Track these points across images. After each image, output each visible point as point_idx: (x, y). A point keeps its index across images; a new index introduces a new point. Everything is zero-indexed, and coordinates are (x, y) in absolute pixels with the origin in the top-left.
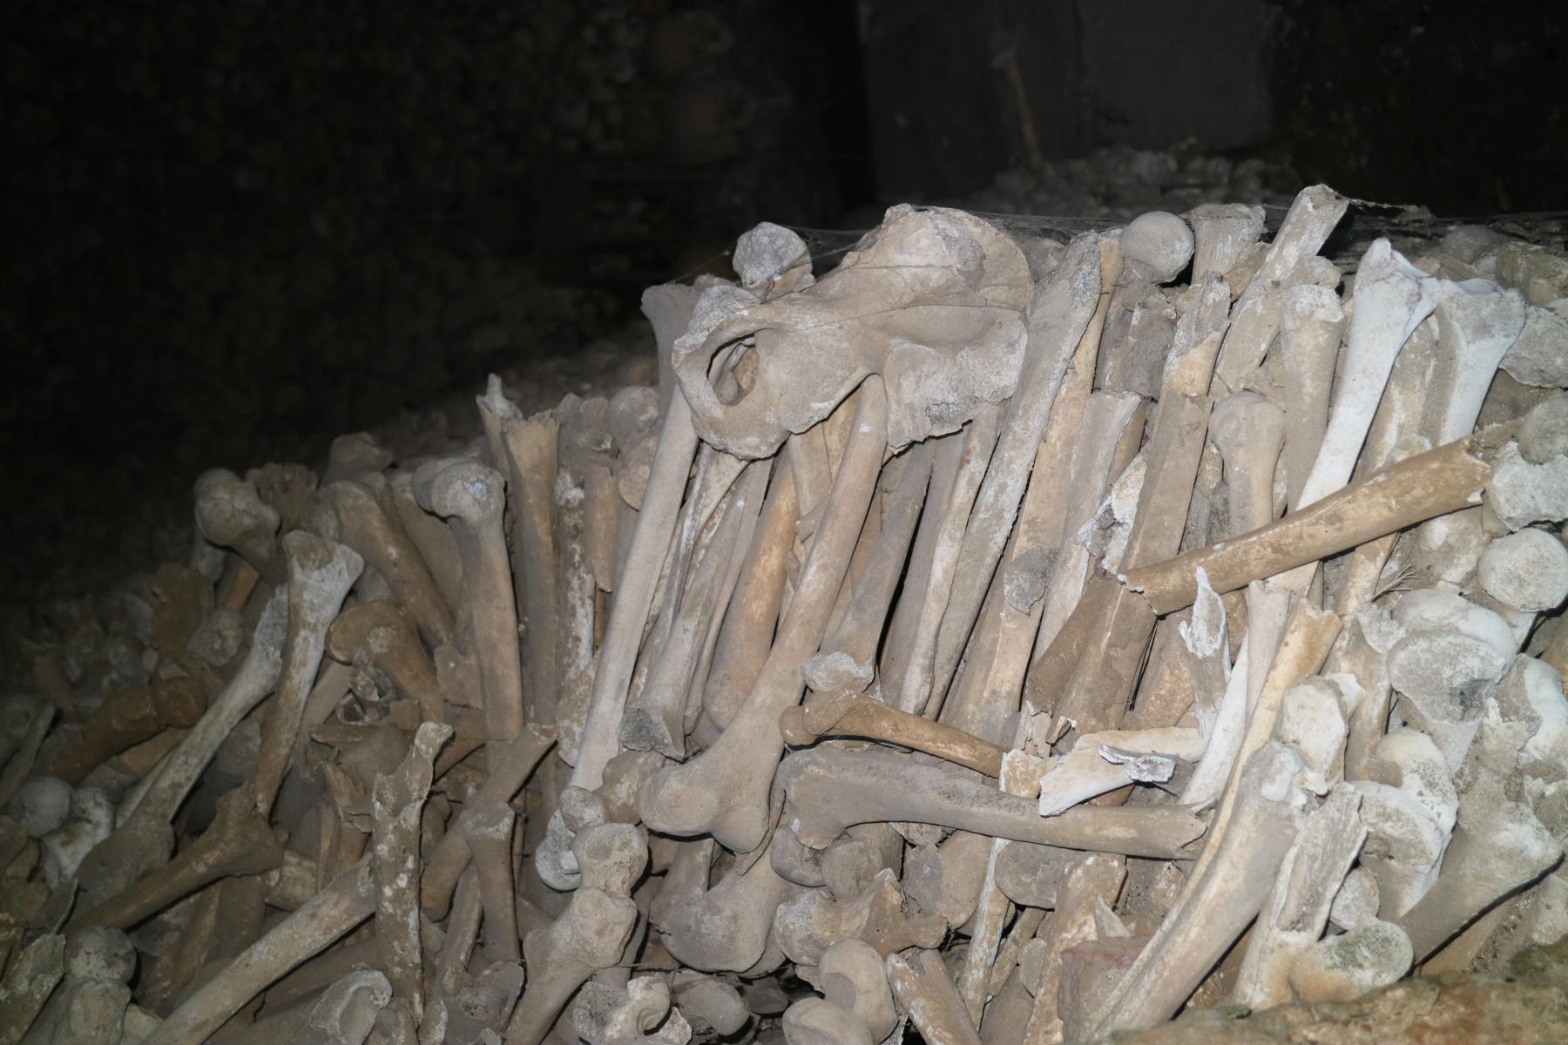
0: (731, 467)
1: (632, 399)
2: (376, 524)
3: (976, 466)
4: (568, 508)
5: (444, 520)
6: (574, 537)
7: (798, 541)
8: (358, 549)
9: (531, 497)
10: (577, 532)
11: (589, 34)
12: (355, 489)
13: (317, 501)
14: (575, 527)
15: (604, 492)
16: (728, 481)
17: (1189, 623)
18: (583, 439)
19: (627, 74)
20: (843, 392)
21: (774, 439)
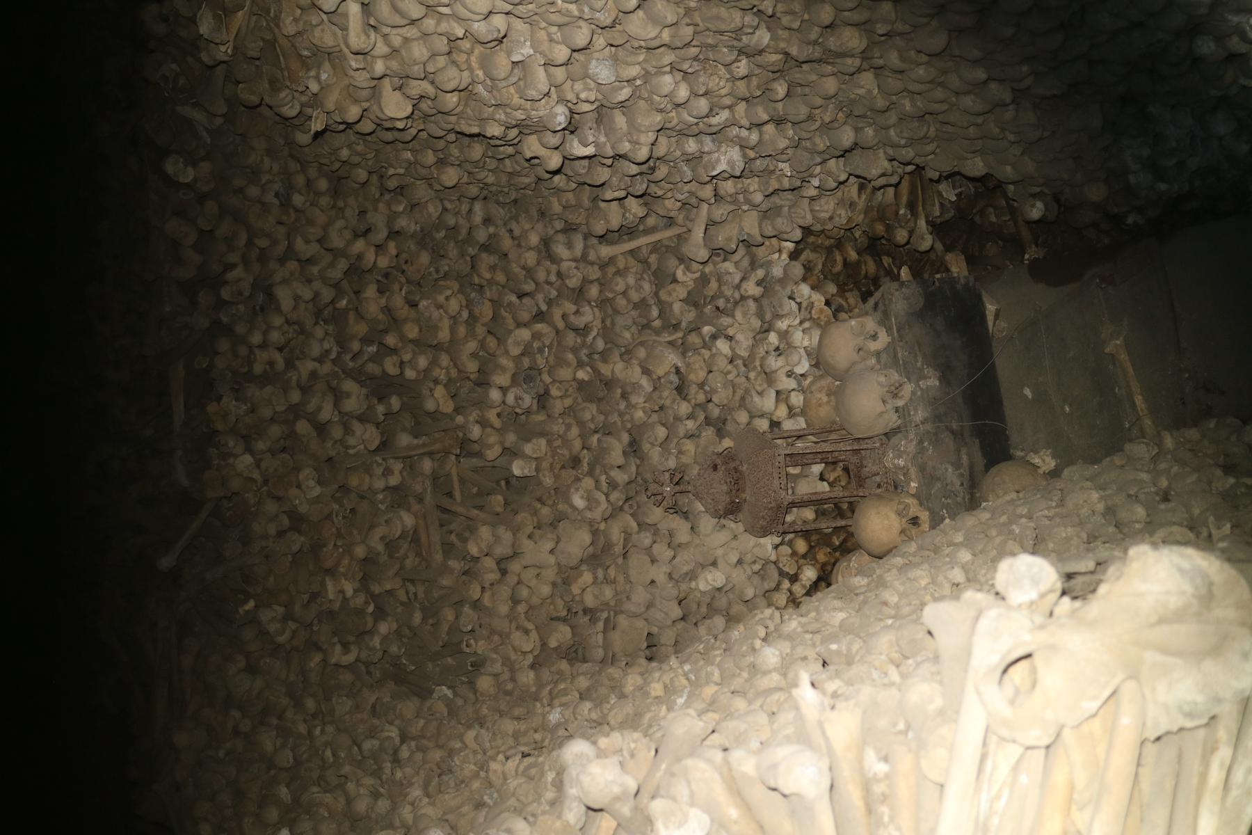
0: (1015, 751)
1: (923, 693)
2: (719, 792)
3: (1224, 753)
4: (876, 779)
5: (785, 796)
6: (883, 802)
7: (1074, 807)
8: (707, 810)
9: (847, 772)
10: (884, 798)
11: (773, 338)
12: (702, 765)
13: (673, 775)
14: (883, 794)
15: (905, 762)
16: (1013, 761)
17: (1076, 586)
18: (883, 723)
19: (803, 367)
20: (1106, 693)
21: (1052, 731)
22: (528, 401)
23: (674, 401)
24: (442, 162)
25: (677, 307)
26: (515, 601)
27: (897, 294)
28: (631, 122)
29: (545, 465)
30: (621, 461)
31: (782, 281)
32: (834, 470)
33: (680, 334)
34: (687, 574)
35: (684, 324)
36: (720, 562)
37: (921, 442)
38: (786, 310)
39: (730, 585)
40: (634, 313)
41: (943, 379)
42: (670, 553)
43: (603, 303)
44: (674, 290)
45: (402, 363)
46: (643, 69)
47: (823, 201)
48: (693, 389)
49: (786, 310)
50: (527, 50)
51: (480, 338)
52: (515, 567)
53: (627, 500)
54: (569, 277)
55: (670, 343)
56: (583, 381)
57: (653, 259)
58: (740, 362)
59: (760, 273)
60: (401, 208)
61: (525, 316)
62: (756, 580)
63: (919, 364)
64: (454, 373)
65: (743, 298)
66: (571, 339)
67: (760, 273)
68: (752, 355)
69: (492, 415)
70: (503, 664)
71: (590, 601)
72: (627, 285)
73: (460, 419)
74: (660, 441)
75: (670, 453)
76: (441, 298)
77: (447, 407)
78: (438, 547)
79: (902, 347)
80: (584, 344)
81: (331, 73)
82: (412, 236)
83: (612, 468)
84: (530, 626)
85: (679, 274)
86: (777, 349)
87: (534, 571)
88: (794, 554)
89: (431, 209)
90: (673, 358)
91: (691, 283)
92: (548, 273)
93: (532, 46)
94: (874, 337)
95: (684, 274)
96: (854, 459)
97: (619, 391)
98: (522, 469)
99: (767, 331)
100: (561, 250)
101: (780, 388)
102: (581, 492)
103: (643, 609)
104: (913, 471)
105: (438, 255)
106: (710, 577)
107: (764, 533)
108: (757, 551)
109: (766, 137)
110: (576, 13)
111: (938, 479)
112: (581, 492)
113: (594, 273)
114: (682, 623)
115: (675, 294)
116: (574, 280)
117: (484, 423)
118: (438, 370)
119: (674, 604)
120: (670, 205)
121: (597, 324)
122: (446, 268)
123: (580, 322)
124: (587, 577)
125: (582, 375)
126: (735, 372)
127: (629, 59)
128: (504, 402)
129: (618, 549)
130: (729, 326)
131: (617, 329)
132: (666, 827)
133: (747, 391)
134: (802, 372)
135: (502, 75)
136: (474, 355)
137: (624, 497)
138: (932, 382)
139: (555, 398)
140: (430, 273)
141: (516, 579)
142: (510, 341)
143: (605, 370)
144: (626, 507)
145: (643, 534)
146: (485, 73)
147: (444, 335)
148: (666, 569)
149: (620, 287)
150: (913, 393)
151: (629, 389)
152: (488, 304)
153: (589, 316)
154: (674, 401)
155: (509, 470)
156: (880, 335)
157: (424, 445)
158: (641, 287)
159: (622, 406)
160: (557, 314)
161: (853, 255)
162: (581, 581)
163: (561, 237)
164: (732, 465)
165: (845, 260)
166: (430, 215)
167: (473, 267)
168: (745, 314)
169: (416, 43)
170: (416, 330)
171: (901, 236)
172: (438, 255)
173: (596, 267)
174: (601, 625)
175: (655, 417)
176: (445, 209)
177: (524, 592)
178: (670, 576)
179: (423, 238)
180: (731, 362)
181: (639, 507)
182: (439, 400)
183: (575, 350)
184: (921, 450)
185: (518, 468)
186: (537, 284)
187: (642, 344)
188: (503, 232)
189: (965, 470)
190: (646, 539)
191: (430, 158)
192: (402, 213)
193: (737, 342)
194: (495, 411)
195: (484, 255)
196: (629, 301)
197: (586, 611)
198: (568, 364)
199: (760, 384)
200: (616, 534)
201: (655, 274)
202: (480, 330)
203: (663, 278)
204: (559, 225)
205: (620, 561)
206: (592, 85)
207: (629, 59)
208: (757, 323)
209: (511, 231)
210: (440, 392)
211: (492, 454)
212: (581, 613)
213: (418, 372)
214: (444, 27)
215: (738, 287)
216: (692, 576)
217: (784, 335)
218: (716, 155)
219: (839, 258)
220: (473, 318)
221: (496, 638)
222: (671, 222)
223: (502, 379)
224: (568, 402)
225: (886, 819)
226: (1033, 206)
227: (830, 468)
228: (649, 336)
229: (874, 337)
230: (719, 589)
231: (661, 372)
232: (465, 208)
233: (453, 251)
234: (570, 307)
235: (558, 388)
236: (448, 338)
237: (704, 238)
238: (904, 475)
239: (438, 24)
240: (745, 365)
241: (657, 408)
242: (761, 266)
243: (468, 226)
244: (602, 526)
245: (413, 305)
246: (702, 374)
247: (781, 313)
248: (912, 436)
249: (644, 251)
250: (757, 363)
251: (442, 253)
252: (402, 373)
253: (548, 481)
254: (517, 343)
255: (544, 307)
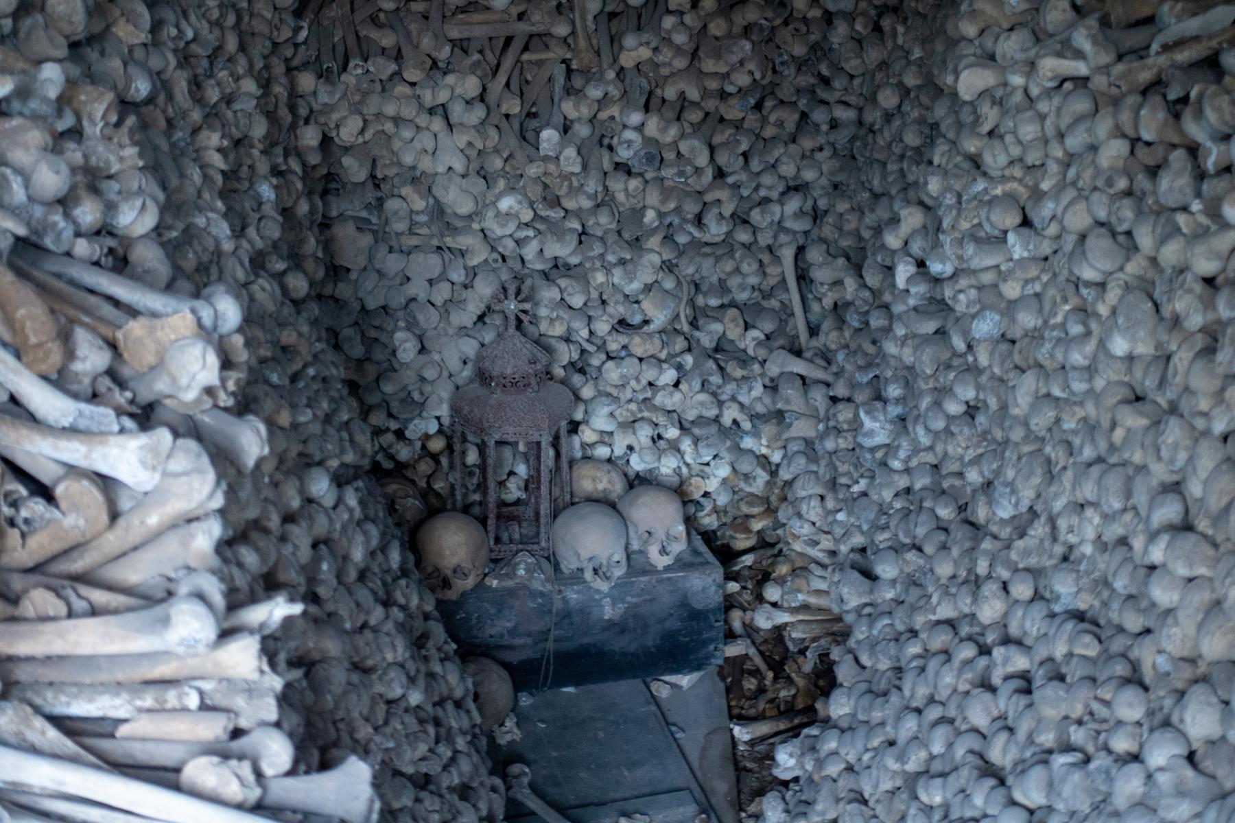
11: (672, 433)
22: (624, 154)
23: (611, 316)
24: (905, 92)
25: (717, 328)
26: (397, 120)
27: (710, 580)
28: (925, 340)
29: (552, 168)
30: (548, 254)
31: (737, 449)
32: (519, 489)
33: (686, 328)
34: (415, 318)
35: (697, 334)
36: (423, 358)
37: (542, 594)
38: (703, 451)
39: (397, 366)
40: (714, 279)
41: (611, 624)
42: (439, 301)
43: (727, 244)
44: (737, 325)
45: (682, 13)
46: (985, 369)
47: (819, 510)
48: (623, 340)
49: (703, 451)
50: (1018, 252)
51: (703, 104)
52: (437, 124)
53: (504, 259)
54: (763, 212)
55: (678, 315)
56: (643, 216)
57: (774, 303)
58: (649, 394)
59: (746, 425)
60: (858, 27)
61: (723, 159)
62: (403, 394)
63: (629, 599)
64: (665, 71)
65: (720, 404)
66: (691, 208)
67: (746, 425)
68: (656, 408)
69: (614, 111)
70: (326, 104)
71: (392, 205)
72: (747, 275)
73: (611, 75)
74: (567, 298)
75: (553, 310)
76: (751, 66)
77: (627, 60)
78: (466, 35)
79: (650, 581)
80: (684, 220)
81: (1018, 10)
82: (825, 37)
83: (542, 243)
84: (368, 135)
85: (755, 333)
86: (660, 437)
87: (430, 145)
88: (427, 437)
89: (855, 62)
90: (660, 318)
91: (742, 347)
92: (769, 188)
93: (1022, 259)
94: (663, 551)
95: (754, 339)
96: (530, 513)
97: (628, 257)
98: (548, 140)
99: (682, 427)
100: (793, 204)
101: (616, 436)
102: (517, 207)
103: (377, 266)
104: (509, 583)
105: (800, 65)
106: (408, 345)
107: (455, 410)
108: (434, 397)
109: (896, 477)
110: (1052, 322)
111: (499, 611)
112: (517, 207)
113: (764, 239)
114: (358, 308)
115: (732, 326)
116: (759, 218)
117: (604, 101)
118: (670, 55)
119: (381, 302)
120: (830, 338)
121: (707, 238)
122: (786, 73)
123: (710, 219)
124: (419, 204)
125: (650, 215)
126: (637, 388)
127: (997, 356)
128: (625, 126)
129: (449, 241)
130: (690, 386)
131: (698, 259)
132: (141, 448)
133: (616, 399)
134: (632, 463)
135: (994, 218)
136: (682, 95)
137: (507, 253)
138: (609, 612)
139: (626, 182)
140: (781, 55)
141: (423, 125)
142: (696, 143)
143: (654, 242)
144: (495, 255)
145: (463, 272)
146: (996, 197)
147: (709, 65)
148: (422, 296)
149: (745, 267)
150: (597, 591)
151: (630, 267)
152: (740, 115)
153: (716, 230)
154: (611, 316)
155: (548, 125)
156: (665, 557)
157: (585, 27)
158: (744, 289)
159: (611, 258)
160: (723, 194)
161: (757, 525)
162: (416, 197)
163: (809, 205)
164: (533, 382)
165: (753, 516)
166: (848, 60)
167: (782, 102)
168: (702, 404)
169: (1039, 129)
170: (718, 33)
171: (772, 593)
172: (800, 65)
173: (770, 242)
174: (364, 214)
175: (595, 295)
176: (852, 77)
177: (407, 134)
178: (414, 299)
179: (819, 50)
180: (650, 384)
181: (494, 270)
182: (635, 51)
183: (678, 210)
184: (533, 594)
185: (549, 136)
186: (758, 174)
187: (679, 283)
188: (821, 140)
189: (507, 640)
190: (458, 275)
191: (911, 80)
192: (853, 29)
193: (671, 394)
194: (616, 114)
195: (796, 116)
196: (730, 274)
197: (381, 201)
198: (663, 202)
199: (623, 414)
200: (463, 241)
201: (757, 304)
202: (711, 104)
203: (749, 314)
204: (822, 204)
205: (435, 242)
206: (973, 310)
207: (997, 356)
208: (691, 415)
209: (821, 149)
210: (645, 53)
211: (568, 108)
212: (379, 194)
213: (669, 32)
214: (1053, 168)
215: (733, 399)
216: (412, 325)
217: (675, 447)
218: (882, 418)
219: (756, 510)
220: (723, 95)
221: (357, 98)
222: (813, 331)
223: (653, 126)
224: (621, 197)
225: (139, 703)
226: (791, 755)
227: (522, 484)
228: (687, 290)
229: (663, 551)
230: (394, 353)
231: (646, 305)
232: (853, 99)
233: (805, 80)
234: (728, 210)
235: (637, 188)
236: (705, 70)
237: (792, 373)
238: (507, 574)
239: (1057, 161)
240: (645, 399)
241: (605, 297)
242: (754, 426)
243: (832, 100)
244: (476, 226)
245: (747, 30)
246: (639, 351)
247: (700, 444)
248: (549, 587)
249: (784, 297)
250: (646, 414)
251: (804, 68)
252: (669, 12)
253: (533, 170)
254: (693, 150)
255: (730, 180)
